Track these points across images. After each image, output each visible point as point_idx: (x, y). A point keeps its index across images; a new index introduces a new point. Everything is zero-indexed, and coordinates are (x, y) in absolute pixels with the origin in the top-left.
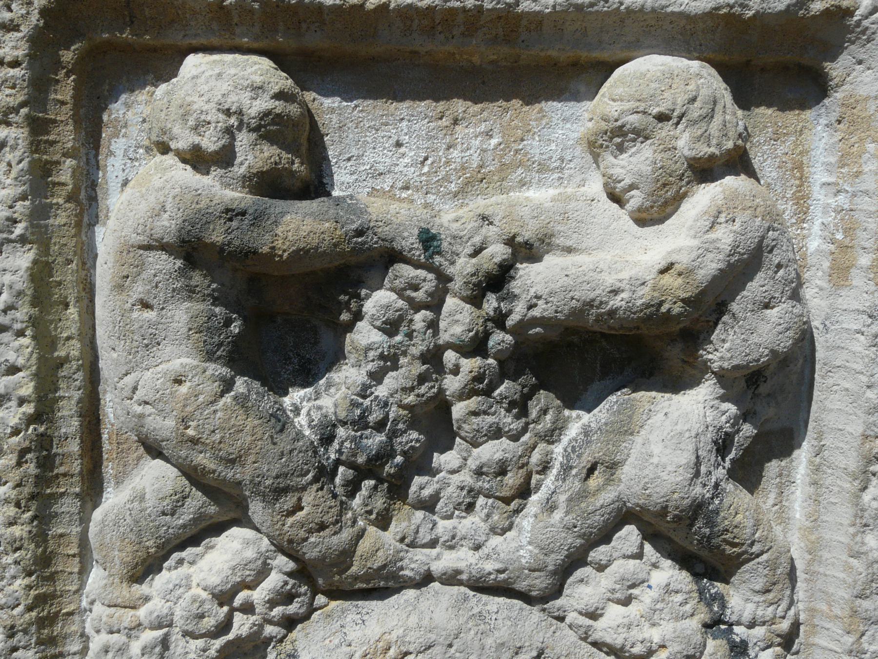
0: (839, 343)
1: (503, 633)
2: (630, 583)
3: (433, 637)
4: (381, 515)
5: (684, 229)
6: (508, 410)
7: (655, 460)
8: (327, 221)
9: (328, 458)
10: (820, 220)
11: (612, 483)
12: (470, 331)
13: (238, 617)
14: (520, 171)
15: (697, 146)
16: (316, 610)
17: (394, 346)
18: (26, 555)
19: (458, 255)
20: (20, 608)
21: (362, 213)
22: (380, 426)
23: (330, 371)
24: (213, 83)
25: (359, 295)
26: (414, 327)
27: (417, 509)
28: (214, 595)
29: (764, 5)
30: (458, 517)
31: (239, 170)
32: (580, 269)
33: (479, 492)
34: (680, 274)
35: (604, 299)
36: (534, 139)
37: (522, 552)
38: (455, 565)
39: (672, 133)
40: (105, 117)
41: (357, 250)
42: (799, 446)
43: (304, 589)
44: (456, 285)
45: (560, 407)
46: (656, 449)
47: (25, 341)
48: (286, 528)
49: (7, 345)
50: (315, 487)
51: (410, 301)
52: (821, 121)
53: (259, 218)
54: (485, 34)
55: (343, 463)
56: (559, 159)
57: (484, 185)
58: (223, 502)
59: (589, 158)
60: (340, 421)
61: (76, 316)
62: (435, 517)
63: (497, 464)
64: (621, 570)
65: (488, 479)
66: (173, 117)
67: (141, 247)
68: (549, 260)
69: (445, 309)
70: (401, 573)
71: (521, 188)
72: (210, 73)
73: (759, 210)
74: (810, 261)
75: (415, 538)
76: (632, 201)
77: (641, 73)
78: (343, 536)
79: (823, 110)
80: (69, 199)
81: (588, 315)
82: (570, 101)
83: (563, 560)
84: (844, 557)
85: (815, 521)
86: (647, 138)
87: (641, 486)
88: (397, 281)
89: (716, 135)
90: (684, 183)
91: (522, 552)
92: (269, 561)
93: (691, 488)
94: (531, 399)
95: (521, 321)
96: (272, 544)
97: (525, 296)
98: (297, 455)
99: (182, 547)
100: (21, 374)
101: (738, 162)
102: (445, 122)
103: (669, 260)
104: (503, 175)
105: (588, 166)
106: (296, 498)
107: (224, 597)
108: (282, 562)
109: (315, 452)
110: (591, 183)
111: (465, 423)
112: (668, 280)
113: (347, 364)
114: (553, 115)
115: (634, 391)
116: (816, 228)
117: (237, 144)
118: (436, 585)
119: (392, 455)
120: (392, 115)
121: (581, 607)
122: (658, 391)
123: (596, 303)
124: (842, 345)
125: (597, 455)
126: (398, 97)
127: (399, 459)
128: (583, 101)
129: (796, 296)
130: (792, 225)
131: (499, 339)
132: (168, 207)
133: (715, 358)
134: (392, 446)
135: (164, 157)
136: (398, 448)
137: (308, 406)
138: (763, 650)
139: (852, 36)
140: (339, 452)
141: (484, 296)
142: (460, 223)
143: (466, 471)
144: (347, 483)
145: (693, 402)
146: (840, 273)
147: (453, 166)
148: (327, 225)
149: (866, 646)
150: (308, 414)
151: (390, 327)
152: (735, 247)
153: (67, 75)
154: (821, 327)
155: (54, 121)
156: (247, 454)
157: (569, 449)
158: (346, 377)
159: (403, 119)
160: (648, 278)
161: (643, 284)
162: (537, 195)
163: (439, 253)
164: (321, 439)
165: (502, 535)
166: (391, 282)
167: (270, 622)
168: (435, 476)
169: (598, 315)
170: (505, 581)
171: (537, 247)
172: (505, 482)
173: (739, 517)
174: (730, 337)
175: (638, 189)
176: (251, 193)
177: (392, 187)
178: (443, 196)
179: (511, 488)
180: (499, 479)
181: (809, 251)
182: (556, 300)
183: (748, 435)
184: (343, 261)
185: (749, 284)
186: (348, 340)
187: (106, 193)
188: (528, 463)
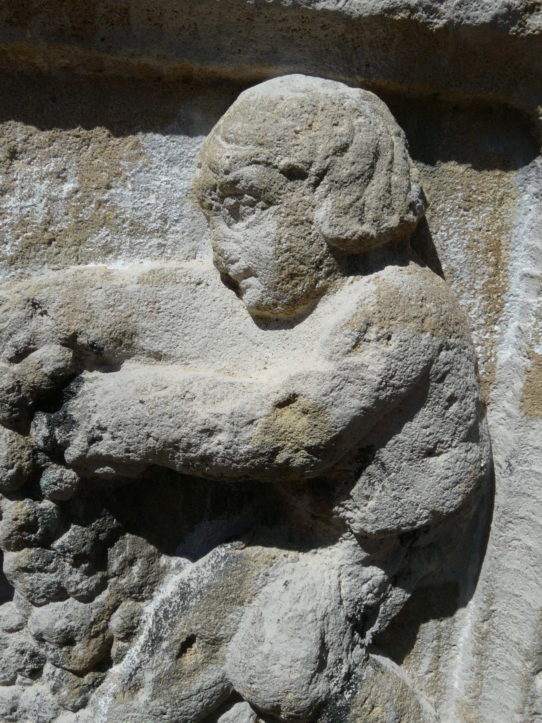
5: (317, 343)
7: (265, 648)
10: (516, 323)
11: (214, 661)
14: (104, 232)
15: (342, 220)
29: (461, 12)
30: (20, 683)
34: (305, 412)
35: (193, 441)
36: (125, 187)
39: (306, 198)
45: (152, 555)
46: (270, 630)
52: (529, 187)
54: (44, 24)
56: (160, 218)
57: (53, 249)
63: (59, 634)
68: (134, 371)
71: (105, 256)
73: (428, 320)
74: (499, 375)
76: (249, 291)
77: (271, 102)
79: (533, 173)
82: (179, 133)
85: (476, 695)
86: (270, 203)
87: (247, 677)
89: (374, 205)
90: (322, 273)
93: (312, 686)
94: (112, 545)
97: (85, 424)
101: (412, 243)
103: (291, 390)
105: (200, 230)
110: (204, 255)
111: (15, 578)
112: (288, 417)
114: (154, 153)
115: (249, 545)
116: (511, 333)
122: (282, 546)
123: (182, 445)
124: (529, 492)
125: (193, 627)
128: (197, 135)
129: (473, 435)
130: (480, 326)
131: (54, 476)
133: (355, 517)
141: (32, 417)
145: (324, 567)
152: (387, 378)
154: (505, 465)
160: (258, 414)
161: (251, 422)
162: (126, 268)
171: (110, 352)
172: (73, 654)
174: (377, 494)
175: (256, 276)
179: (82, 661)
180: (64, 649)
181: (499, 363)
182: (126, 435)
183: (397, 602)
185: (407, 425)
188: (106, 628)
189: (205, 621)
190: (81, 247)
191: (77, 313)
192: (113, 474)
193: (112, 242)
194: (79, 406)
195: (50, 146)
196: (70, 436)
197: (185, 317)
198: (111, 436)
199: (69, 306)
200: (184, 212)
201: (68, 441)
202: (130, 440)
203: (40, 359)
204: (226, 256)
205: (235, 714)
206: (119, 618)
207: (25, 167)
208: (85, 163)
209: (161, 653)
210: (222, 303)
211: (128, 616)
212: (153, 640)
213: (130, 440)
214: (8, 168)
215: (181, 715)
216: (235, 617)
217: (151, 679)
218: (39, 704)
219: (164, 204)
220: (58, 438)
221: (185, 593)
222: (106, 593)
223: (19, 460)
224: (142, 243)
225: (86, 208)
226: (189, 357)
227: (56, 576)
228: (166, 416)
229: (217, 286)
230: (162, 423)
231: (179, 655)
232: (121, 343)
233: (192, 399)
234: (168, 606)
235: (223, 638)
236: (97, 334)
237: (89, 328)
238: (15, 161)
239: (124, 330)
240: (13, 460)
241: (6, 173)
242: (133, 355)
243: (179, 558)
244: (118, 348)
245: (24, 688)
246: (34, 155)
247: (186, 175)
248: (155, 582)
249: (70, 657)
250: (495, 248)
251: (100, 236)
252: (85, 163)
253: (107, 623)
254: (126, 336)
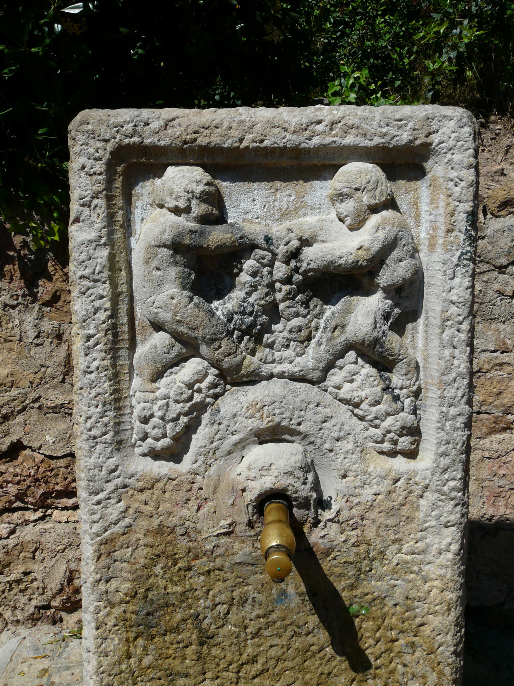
0: (432, 275)
1: (303, 396)
3: (275, 399)
6: (301, 306)
7: (359, 323)
13: (196, 394)
14: (303, 209)
16: (227, 391)
18: (109, 372)
20: (108, 394)
22: (251, 314)
24: (181, 180)
28: (187, 385)
31: (193, 215)
40: (133, 192)
41: (240, 245)
42: (420, 317)
43: (222, 382)
44: (279, 257)
46: (360, 318)
47: (106, 285)
49: (99, 287)
50: (226, 338)
51: (262, 264)
53: (202, 233)
57: (289, 216)
58: (188, 346)
61: (125, 275)
66: (166, 194)
67: (156, 246)
68: (315, 246)
69: (275, 266)
72: (179, 176)
74: (421, 242)
80: (121, 227)
84: (437, 360)
85: (426, 346)
86: (351, 197)
95: (305, 270)
96: (209, 363)
99: (171, 367)
100: (105, 299)
101: (391, 204)
102: (272, 190)
107: (190, 386)
112: (361, 252)
116: (424, 229)
117: (192, 204)
119: (256, 325)
121: (333, 385)
126: (254, 181)
127: (259, 327)
132: (167, 230)
135: (162, 210)
136: (258, 322)
137: (220, 307)
138: (406, 398)
139: (433, 153)
140: (235, 325)
146: (432, 247)
149: (446, 394)
151: (254, 274)
153: (119, 177)
155: (115, 196)
156: (200, 326)
163: (272, 245)
167: (208, 396)
170: (303, 375)
173: (393, 344)
176: (198, 223)
187: (135, 224)
222: (310, 316)
250: (416, 204)
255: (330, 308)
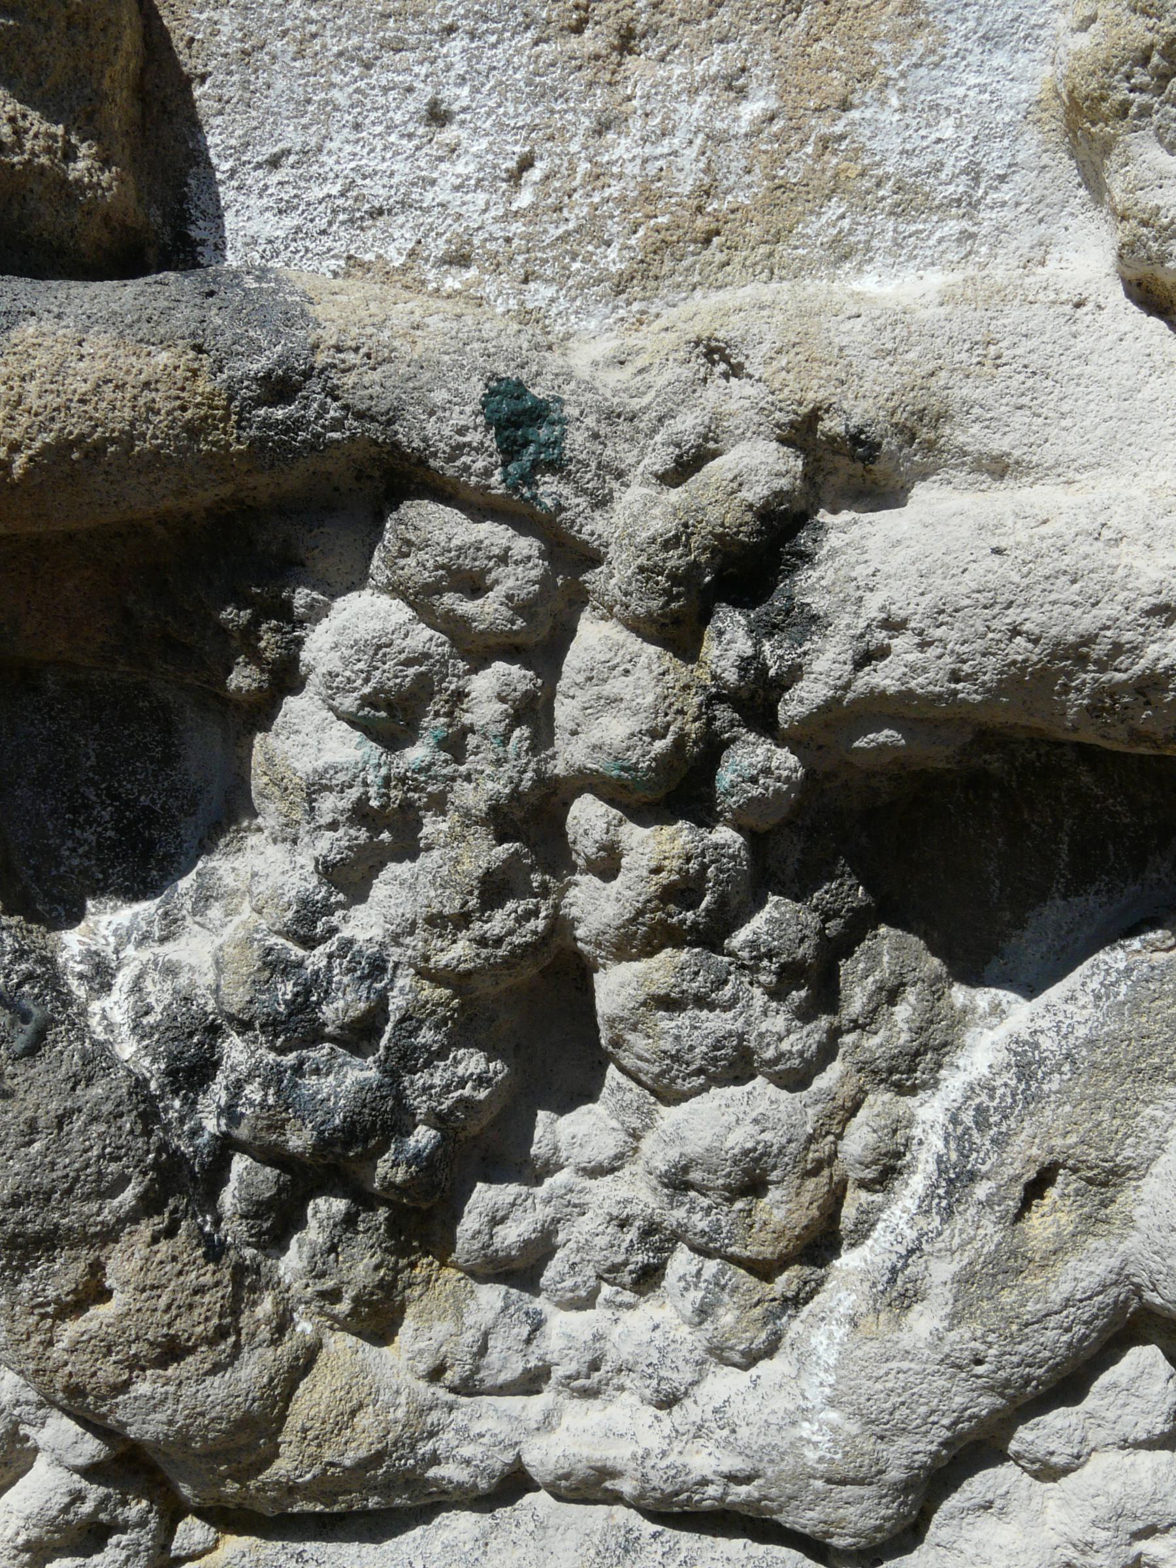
2: (1141, 1525)
4: (369, 1304)
6: (776, 994)
8: (164, 343)
9: (196, 1132)
11: (1101, 1228)
12: (656, 734)
14: (834, 208)
17: (403, 779)
19: (619, 475)
21: (289, 321)
22: (360, 1035)
23: (210, 852)
25: (288, 605)
26: (467, 719)
27: (484, 1279)
30: (609, 1303)
32: (1045, 530)
33: (677, 1236)
35: (1128, 636)
37: (806, 1429)
38: (597, 1455)
41: (270, 451)
43: (136, 1509)
44: (612, 578)
45: (939, 978)
48: (57, 1352)
50: (146, 1229)
51: (455, 628)
55: (243, 1147)
56: (965, 171)
57: (714, 253)
59: (1066, 168)
60: (231, 1018)
62: (539, 1303)
64: (1115, 1487)
65: (705, 1202)
68: (926, 498)
69: (575, 658)
70: (432, 1473)
75: (477, 1369)
78: (243, 1374)
81: (1066, 689)
83: (935, 1455)
88: (411, 561)
91: (806, 1429)
92: (24, 1430)
94: (849, 954)
95: (830, 706)
97: (847, 619)
98: (82, 1132)
102: (591, 41)
104: (779, 220)
105: (1059, 196)
106: (81, 1266)
108: (59, 1434)
109: (149, 1116)
111: (634, 1028)
113: (260, 829)
114: (951, 21)
118: (539, 1500)
119: (398, 1122)
120: (416, 15)
123: (1099, 650)
125: (1058, 1142)
127: (423, 1137)
134: (400, 1097)
136: (421, 1105)
140: (229, 1112)
141: (706, 617)
142: (630, 369)
143: (639, 1168)
144: (256, 1210)
147: (614, 191)
148: (164, 358)
150: (137, 987)
151: (389, 717)
157: (967, 1118)
158: (254, 875)
159: (451, 29)
163: (556, 467)
164: (171, 1073)
165: (745, 1367)
166: (391, 564)
168: (538, 1181)
169: (1099, 692)
172: (759, 1216)
177: (412, 254)
178: (581, 287)
179: (779, 1235)
180: (739, 1205)
182: (954, 635)
184: (226, 490)
186: (257, 756)
188: (834, 1155)
189: (1088, 1125)
190: (780, 247)
191: (815, 365)
192: (896, 748)
193: (851, 232)
194: (823, 583)
195: (710, 17)
196: (805, 653)
197: (1059, 377)
198: (917, 640)
199: (797, 349)
200: (1020, 158)
201: (800, 666)
202: (965, 648)
203: (736, 472)
204: (1165, 221)
205: (1133, 1373)
206: (866, 1129)
207: (652, 68)
208: (792, 51)
209: (973, 1211)
210: (1138, 345)
211: (886, 1126)
212: (950, 1181)
213: (965, 648)
214: (613, 73)
215: (1019, 1365)
216: (1159, 1113)
217: (947, 1276)
218: (660, 1350)
219: (975, 138)
220: (770, 663)
221: (1030, 1064)
222: (836, 1068)
223: (680, 718)
224: (921, 232)
225: (794, 155)
226: (1076, 464)
227: (735, 1019)
228: (1063, 578)
229: (1121, 308)
230: (1053, 597)
231: (1019, 1217)
232: (913, 437)
233: (1117, 541)
234: (984, 1098)
235: (1129, 1168)
236: (866, 411)
237: (846, 398)
238: (629, 58)
239: (921, 406)
240: (666, 715)
241: (610, 84)
242: (934, 472)
243: (993, 990)
244: (905, 451)
245: (618, 1314)
246: (675, 39)
247: (1025, 69)
248: (945, 1044)
249: (751, 1226)
251: (824, 219)
252: (792, 51)
253: (835, 1143)
254: (925, 421)
255: (997, 1010)
